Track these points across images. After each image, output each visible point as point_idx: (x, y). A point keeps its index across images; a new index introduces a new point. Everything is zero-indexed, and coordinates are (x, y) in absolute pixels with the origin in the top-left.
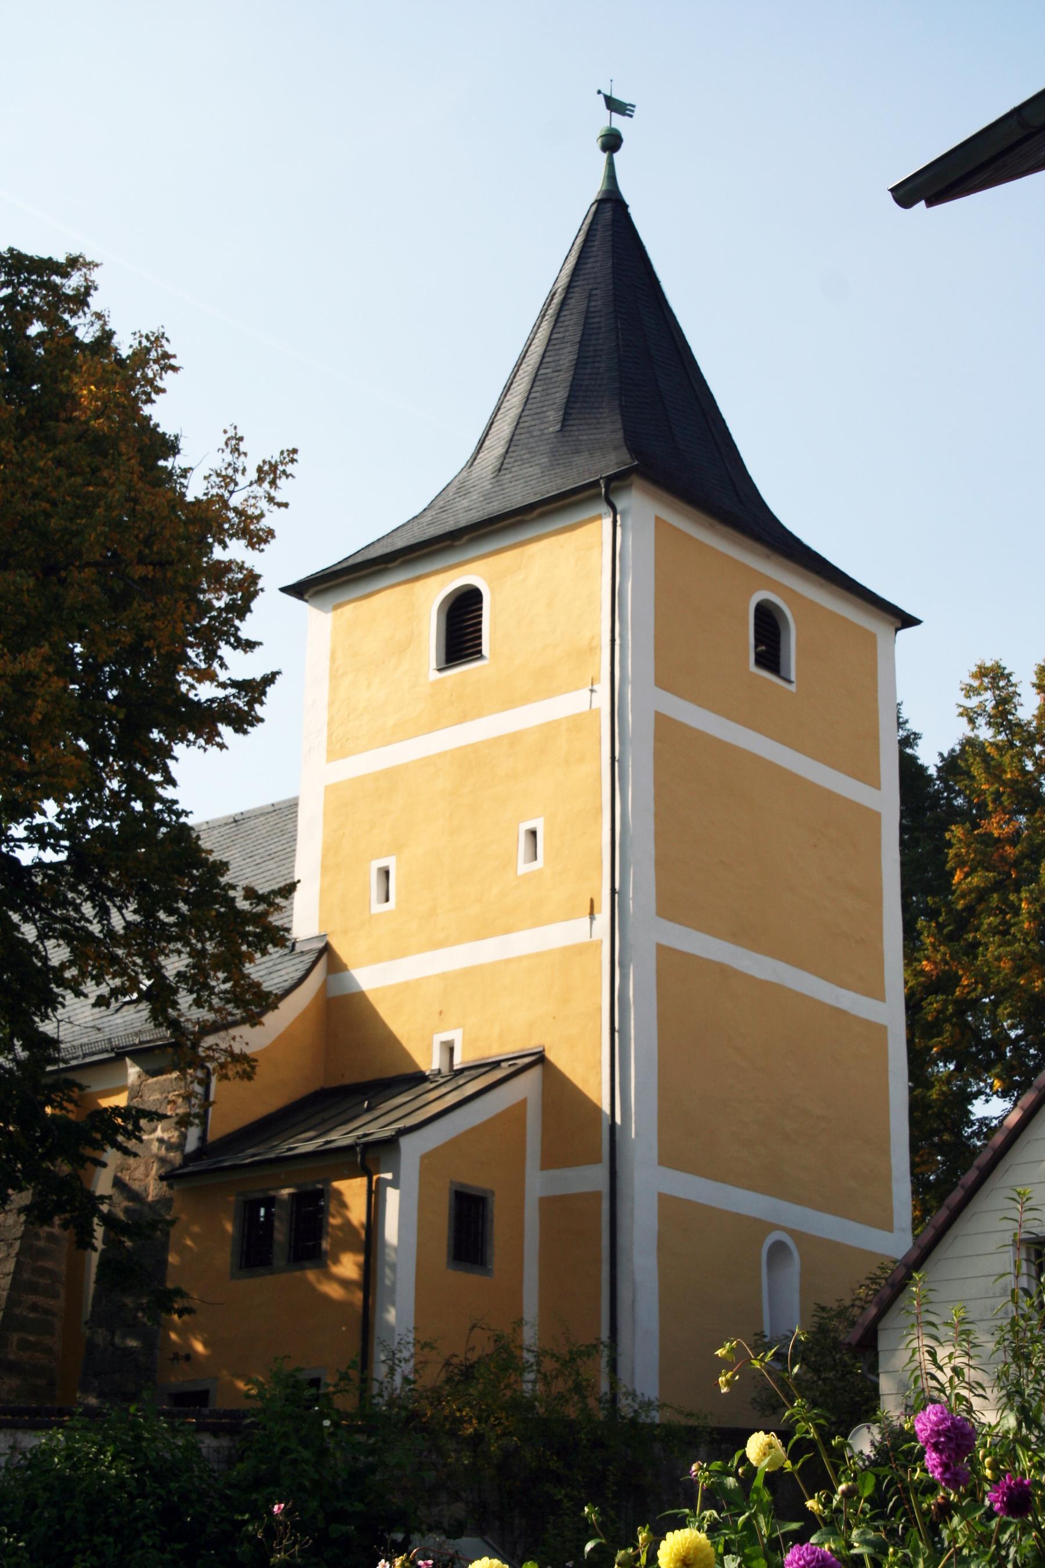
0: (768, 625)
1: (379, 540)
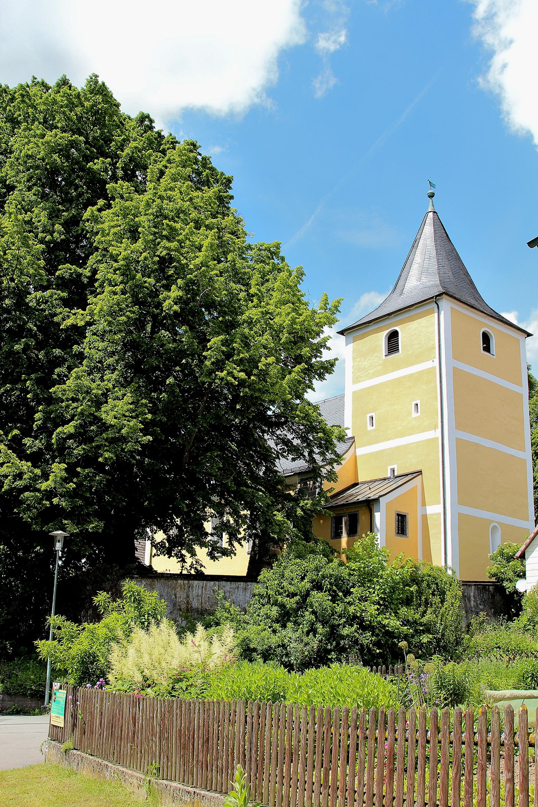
0: (486, 338)
1: (472, 282)
